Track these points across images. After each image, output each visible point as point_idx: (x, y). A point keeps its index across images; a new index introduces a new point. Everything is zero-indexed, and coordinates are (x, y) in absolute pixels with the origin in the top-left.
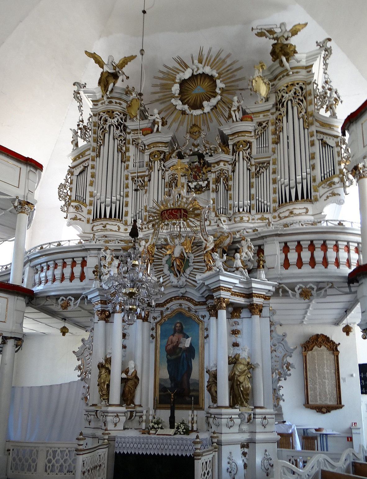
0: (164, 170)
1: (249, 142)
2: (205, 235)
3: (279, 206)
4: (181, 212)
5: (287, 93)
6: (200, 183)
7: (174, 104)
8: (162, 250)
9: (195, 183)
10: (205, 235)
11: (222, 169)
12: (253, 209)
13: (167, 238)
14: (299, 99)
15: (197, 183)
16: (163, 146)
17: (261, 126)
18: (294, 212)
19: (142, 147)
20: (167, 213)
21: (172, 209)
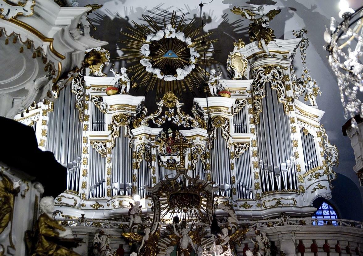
0: (131, 137)
1: (227, 119)
2: (157, 215)
3: (263, 193)
4: (192, 198)
5: (265, 75)
6: (175, 157)
7: (144, 65)
8: (164, 240)
9: (168, 157)
10: (157, 215)
11: (199, 145)
12: (235, 194)
13: (173, 226)
14: (278, 83)
15: (170, 157)
16: (130, 109)
17: (238, 103)
18: (282, 203)
19: (103, 106)
20: (176, 197)
21: (182, 194)
